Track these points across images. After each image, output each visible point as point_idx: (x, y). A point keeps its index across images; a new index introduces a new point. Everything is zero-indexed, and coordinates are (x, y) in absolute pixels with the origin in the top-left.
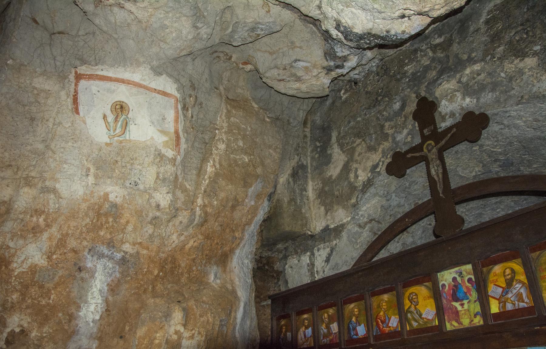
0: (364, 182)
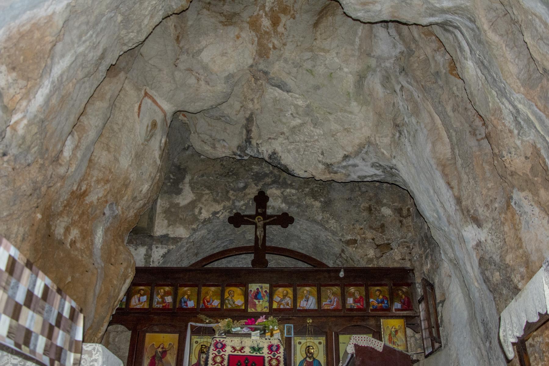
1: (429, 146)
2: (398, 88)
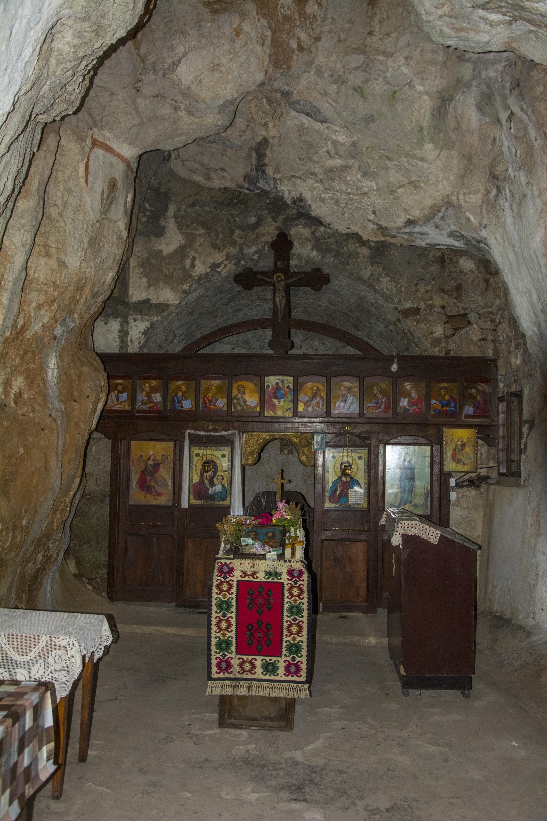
2: (504, 116)
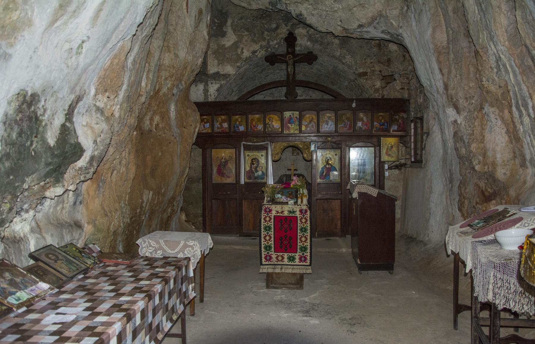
0: (247, 57)
1: (429, 32)
